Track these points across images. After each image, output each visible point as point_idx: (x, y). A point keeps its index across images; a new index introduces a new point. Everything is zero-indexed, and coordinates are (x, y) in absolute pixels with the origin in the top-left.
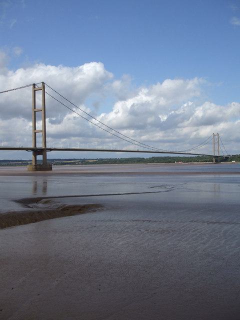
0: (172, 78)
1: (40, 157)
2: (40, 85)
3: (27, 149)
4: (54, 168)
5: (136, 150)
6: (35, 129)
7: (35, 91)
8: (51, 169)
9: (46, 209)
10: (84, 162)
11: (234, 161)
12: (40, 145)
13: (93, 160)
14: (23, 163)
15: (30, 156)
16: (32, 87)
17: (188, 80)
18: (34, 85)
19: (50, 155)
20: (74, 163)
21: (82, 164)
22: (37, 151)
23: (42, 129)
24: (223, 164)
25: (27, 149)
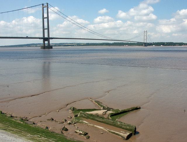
0: (110, 16)
1: (46, 42)
2: (46, 5)
3: (40, 38)
4: (53, 47)
5: (25, 36)
6: (44, 28)
7: (43, 8)
8: (52, 48)
9: (9, 51)
10: (79, 45)
11: (154, 46)
12: (46, 36)
13: (83, 43)
14: (36, 45)
15: (41, 41)
16: (42, 5)
17: (178, 10)
18: (43, 4)
19: (52, 42)
20: (73, 45)
21: (77, 46)
22: (45, 39)
23: (47, 28)
24: (149, 47)
25: (40, 38)
